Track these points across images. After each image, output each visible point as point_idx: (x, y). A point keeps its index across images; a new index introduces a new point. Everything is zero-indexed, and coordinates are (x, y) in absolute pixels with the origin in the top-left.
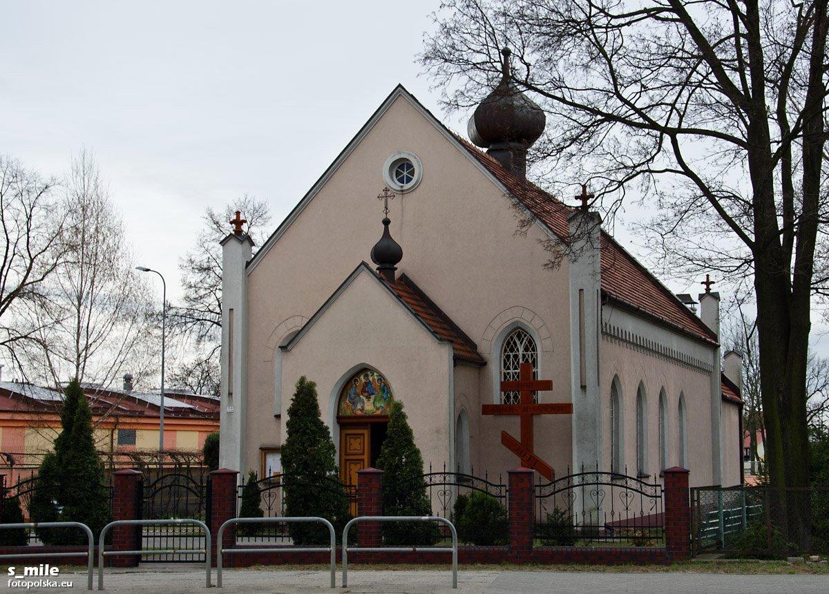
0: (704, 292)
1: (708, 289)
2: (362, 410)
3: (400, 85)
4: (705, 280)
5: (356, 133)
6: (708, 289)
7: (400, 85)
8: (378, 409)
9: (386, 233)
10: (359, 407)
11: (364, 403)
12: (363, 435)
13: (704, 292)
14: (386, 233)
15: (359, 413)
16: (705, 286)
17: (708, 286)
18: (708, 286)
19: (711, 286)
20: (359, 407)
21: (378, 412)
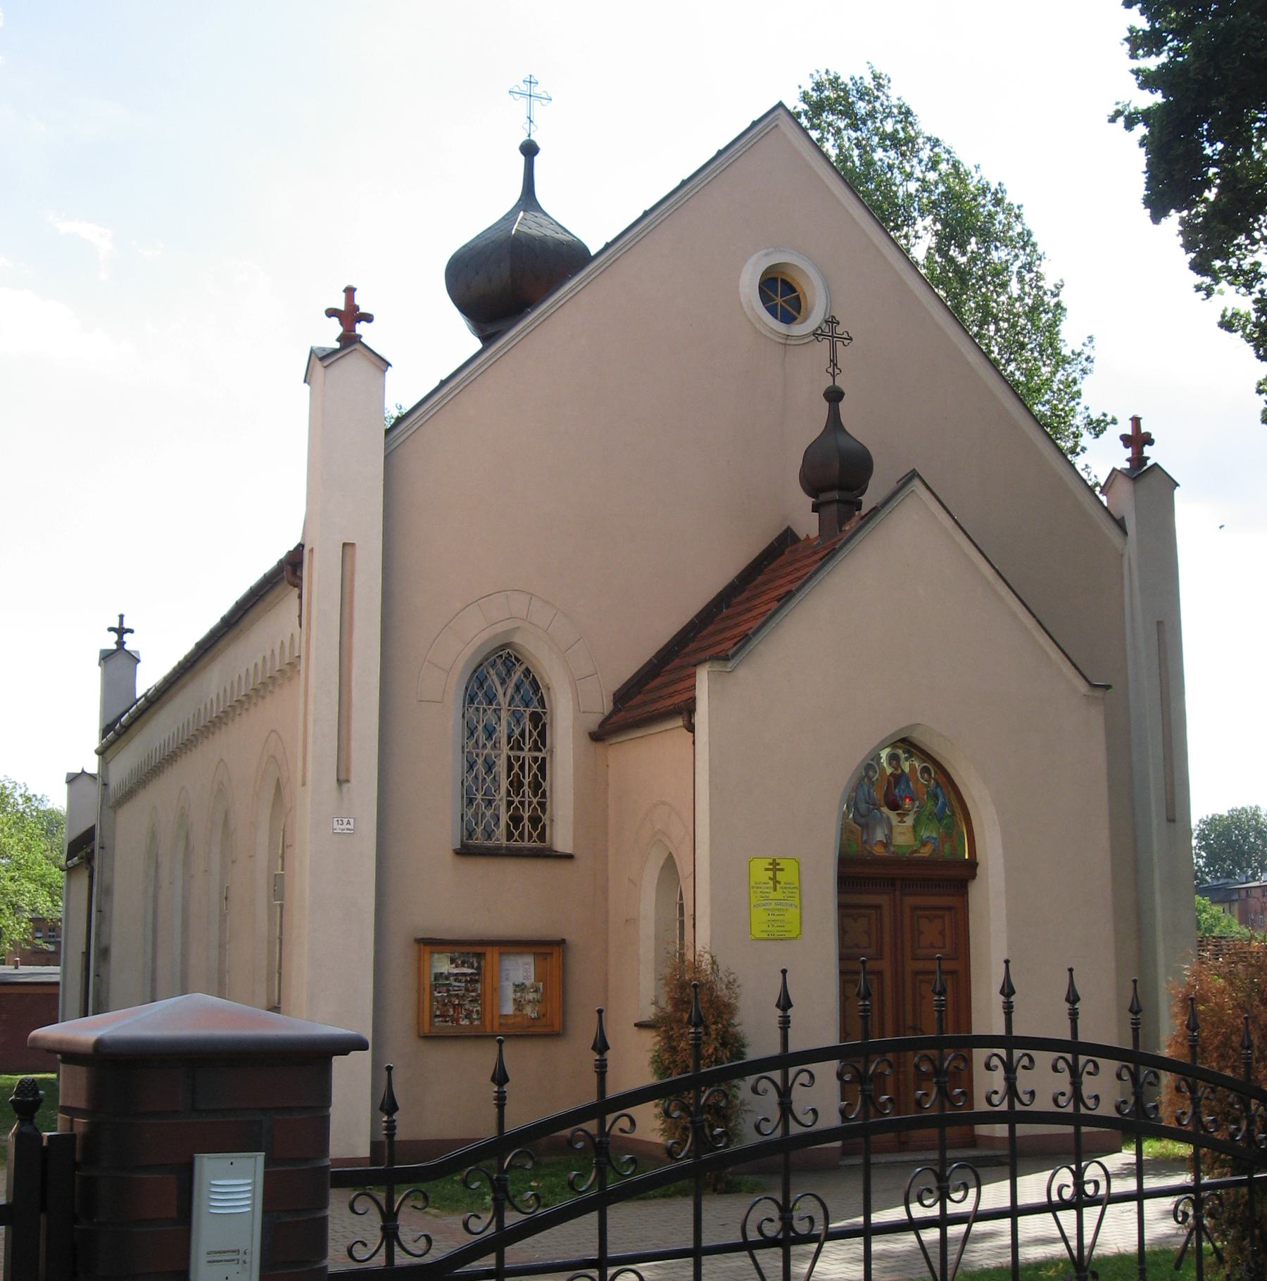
0: (114, 647)
1: (121, 643)
2: (885, 845)
3: (344, 544)
4: (117, 626)
5: (704, 1224)
6: (121, 643)
7: (344, 544)
8: (924, 844)
9: (834, 421)
10: (880, 835)
11: (891, 828)
12: (878, 907)
13: (114, 647)
14: (834, 421)
15: (879, 851)
16: (114, 636)
17: (121, 637)
18: (121, 637)
19: (126, 637)
20: (880, 835)
21: (925, 852)
